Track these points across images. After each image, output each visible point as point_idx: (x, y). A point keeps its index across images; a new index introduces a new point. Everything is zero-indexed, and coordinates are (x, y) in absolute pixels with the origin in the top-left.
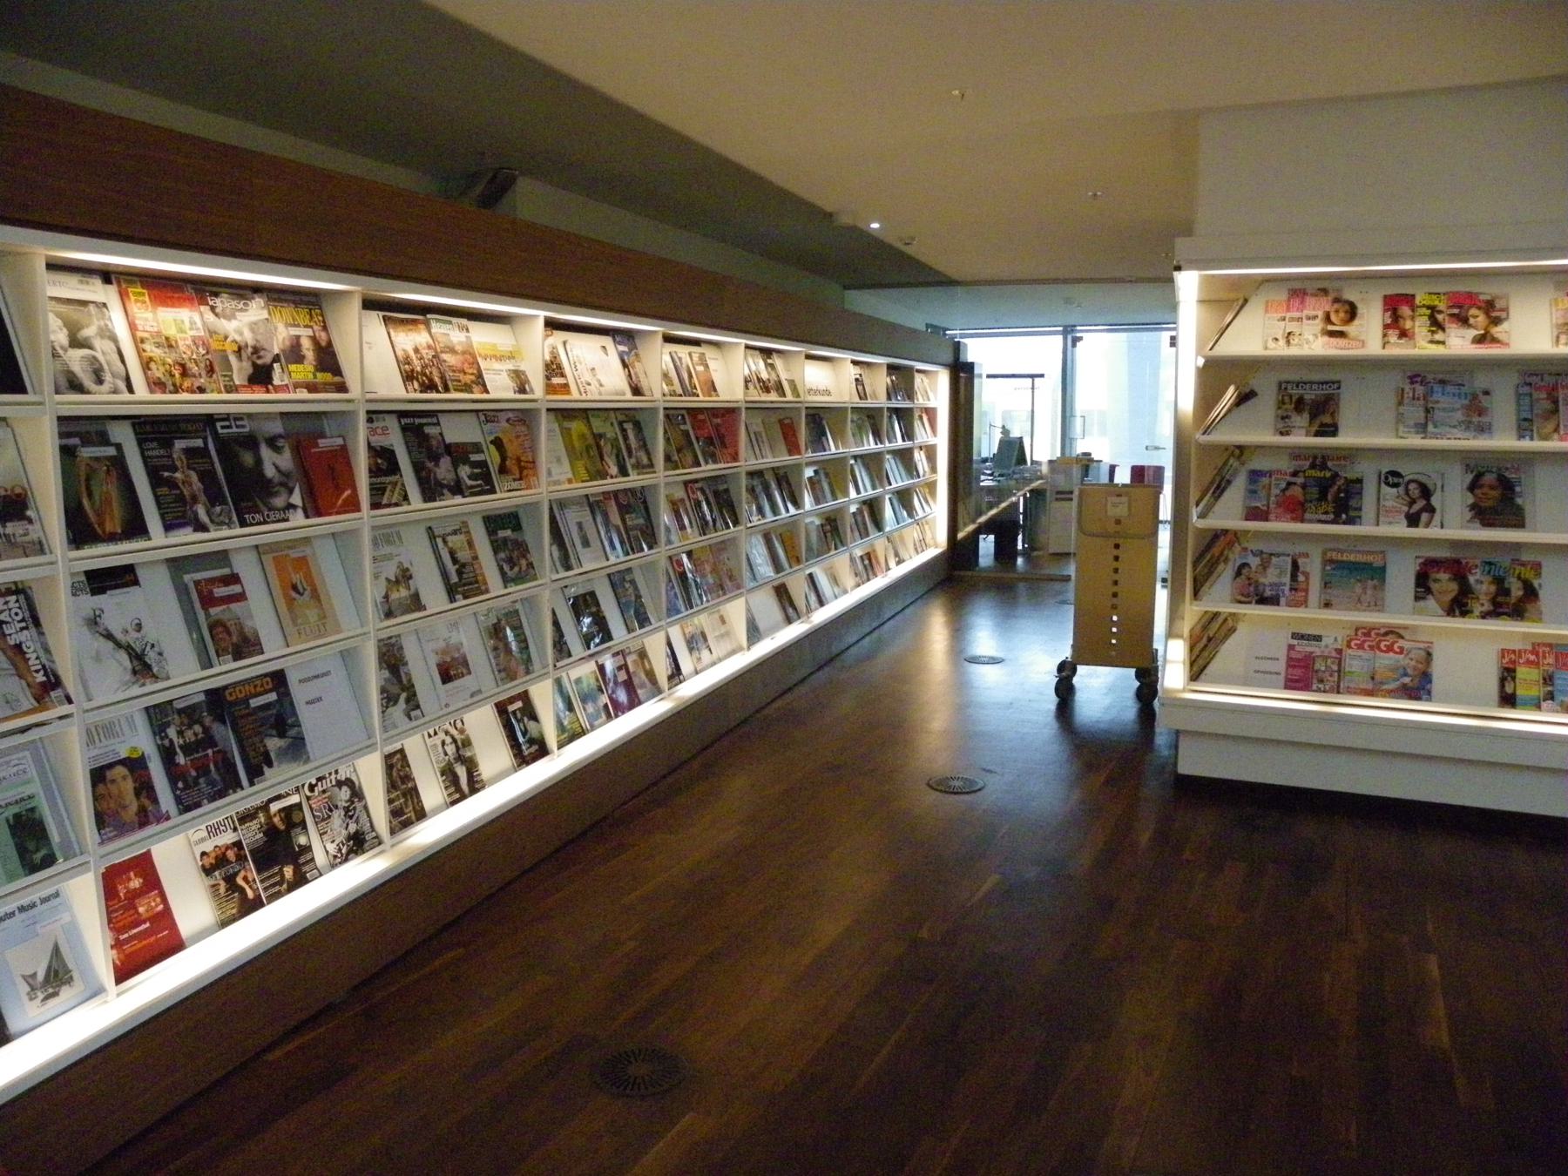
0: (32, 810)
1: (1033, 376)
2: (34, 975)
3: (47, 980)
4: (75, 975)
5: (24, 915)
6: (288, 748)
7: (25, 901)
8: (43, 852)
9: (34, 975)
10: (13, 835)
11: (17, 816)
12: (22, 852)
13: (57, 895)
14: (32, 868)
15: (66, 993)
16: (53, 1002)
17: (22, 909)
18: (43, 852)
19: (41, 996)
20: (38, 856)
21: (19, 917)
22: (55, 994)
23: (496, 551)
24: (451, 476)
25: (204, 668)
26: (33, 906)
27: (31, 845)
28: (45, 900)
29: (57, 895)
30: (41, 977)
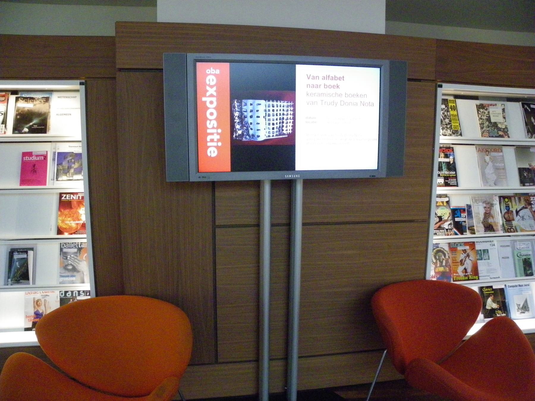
0: (529, 259)
1: (215, 227)
2: (519, 305)
3: (522, 308)
4: (530, 309)
5: (520, 287)
6: (494, 296)
7: (521, 284)
8: (530, 271)
9: (519, 305)
10: (524, 264)
11: (525, 259)
12: (525, 270)
13: (529, 285)
14: (527, 275)
15: (527, 313)
16: (523, 314)
17: (520, 286)
18: (530, 271)
19: (520, 311)
20: (529, 272)
21: (518, 287)
22: (524, 313)
23: (455, 243)
24: (238, 113)
25: (5, 285)
26: (522, 286)
27: (527, 268)
28: (526, 285)
29: (529, 285)
30: (521, 306)
